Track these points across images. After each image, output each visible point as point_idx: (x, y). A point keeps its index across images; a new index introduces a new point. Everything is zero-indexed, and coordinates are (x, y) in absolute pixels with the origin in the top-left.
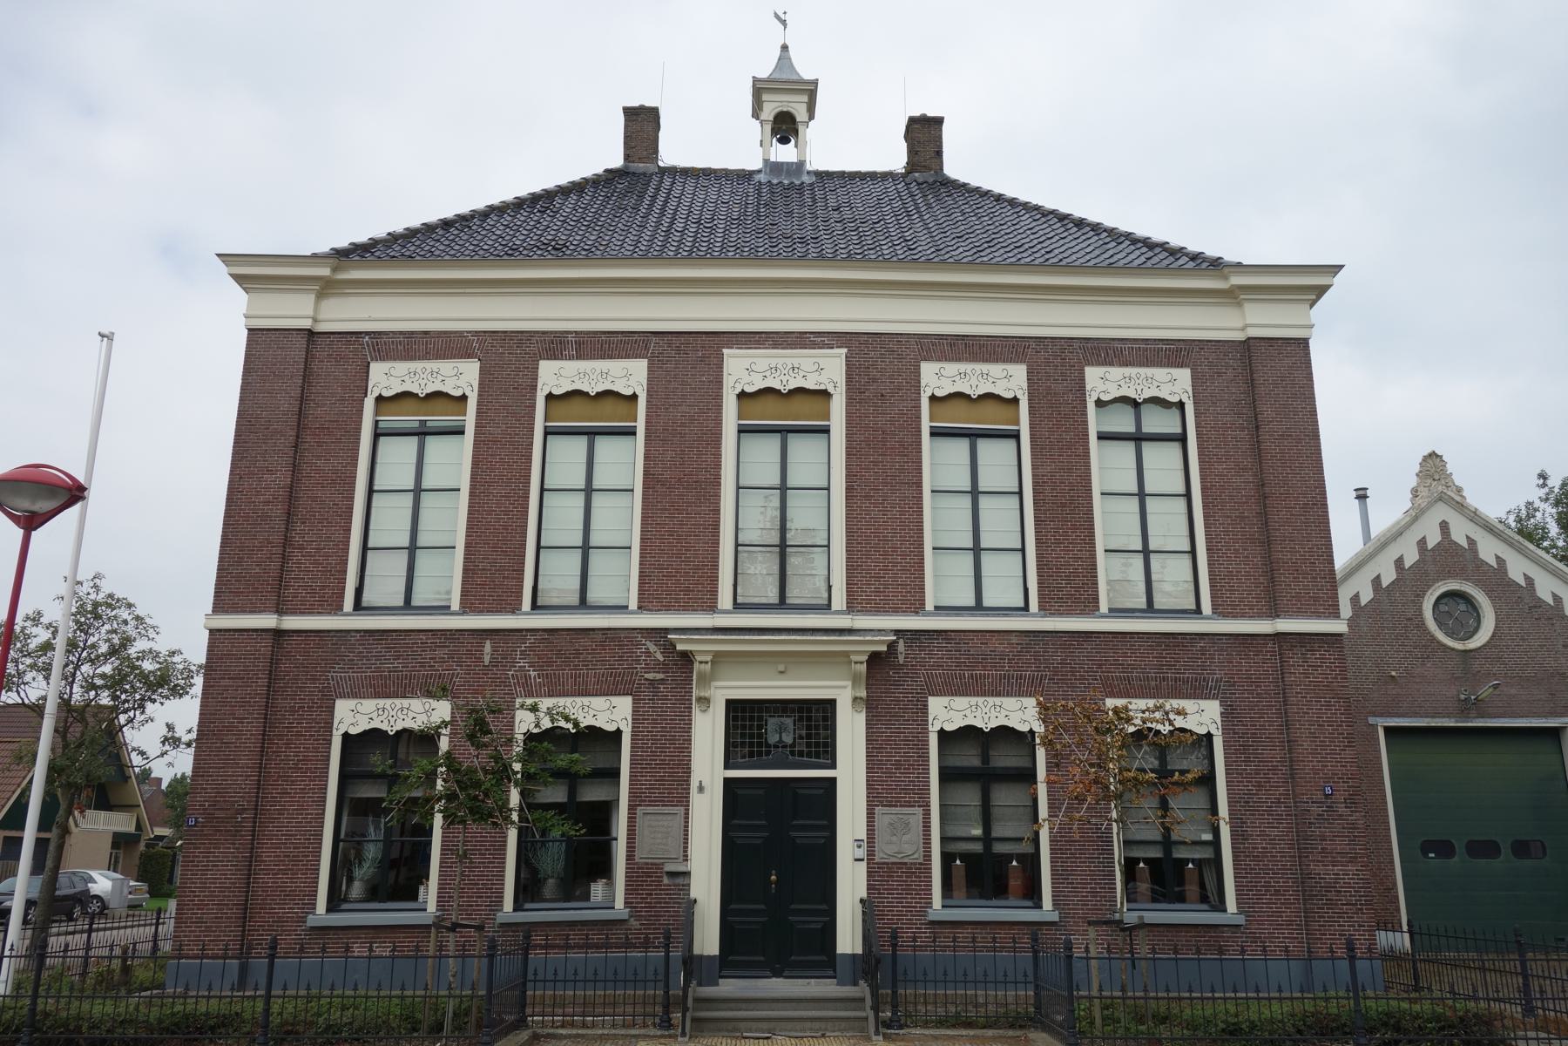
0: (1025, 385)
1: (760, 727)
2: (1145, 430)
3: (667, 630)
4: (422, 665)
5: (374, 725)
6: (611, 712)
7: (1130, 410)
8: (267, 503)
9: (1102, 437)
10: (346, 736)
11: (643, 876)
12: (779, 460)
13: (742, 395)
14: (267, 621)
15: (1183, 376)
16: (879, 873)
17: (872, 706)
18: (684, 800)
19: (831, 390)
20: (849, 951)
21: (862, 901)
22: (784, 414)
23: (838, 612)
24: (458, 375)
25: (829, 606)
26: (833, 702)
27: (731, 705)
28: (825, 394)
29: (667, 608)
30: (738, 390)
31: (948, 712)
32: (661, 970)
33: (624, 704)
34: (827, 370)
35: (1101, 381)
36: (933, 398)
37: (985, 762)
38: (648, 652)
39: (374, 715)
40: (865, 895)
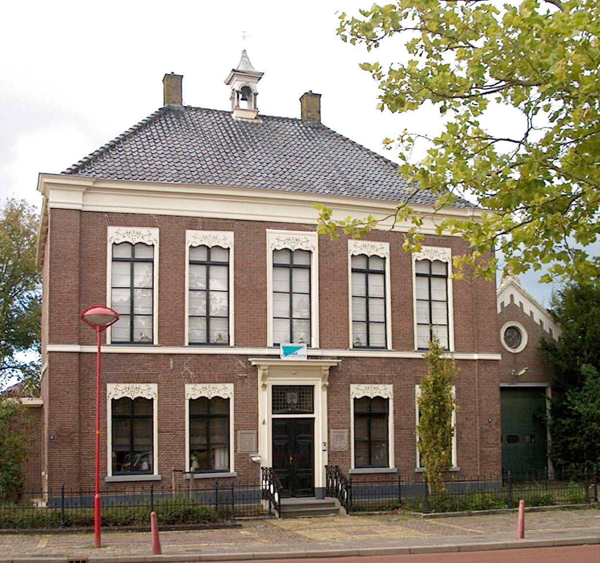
0: (389, 252)
1: (284, 397)
2: (212, 260)
3: (247, 355)
4: (144, 369)
5: (125, 395)
6: (226, 391)
7: (130, 246)
8: (69, 293)
9: (417, 275)
10: (113, 400)
11: (242, 458)
12: (289, 280)
13: (275, 251)
14: (76, 348)
15: (387, 245)
16: (332, 454)
17: (330, 390)
18: (256, 427)
19: (312, 251)
20: (321, 486)
21: (326, 466)
22: (291, 262)
23: (232, 347)
24: (150, 235)
25: (152, 343)
26: (313, 387)
27: (275, 388)
28: (310, 252)
29: (246, 345)
30: (273, 249)
31: (358, 391)
32: (398, 490)
33: (154, 387)
34: (310, 241)
35: (193, 237)
36: (191, 247)
37: (371, 412)
38: (240, 365)
39: (124, 391)
40: (327, 464)
